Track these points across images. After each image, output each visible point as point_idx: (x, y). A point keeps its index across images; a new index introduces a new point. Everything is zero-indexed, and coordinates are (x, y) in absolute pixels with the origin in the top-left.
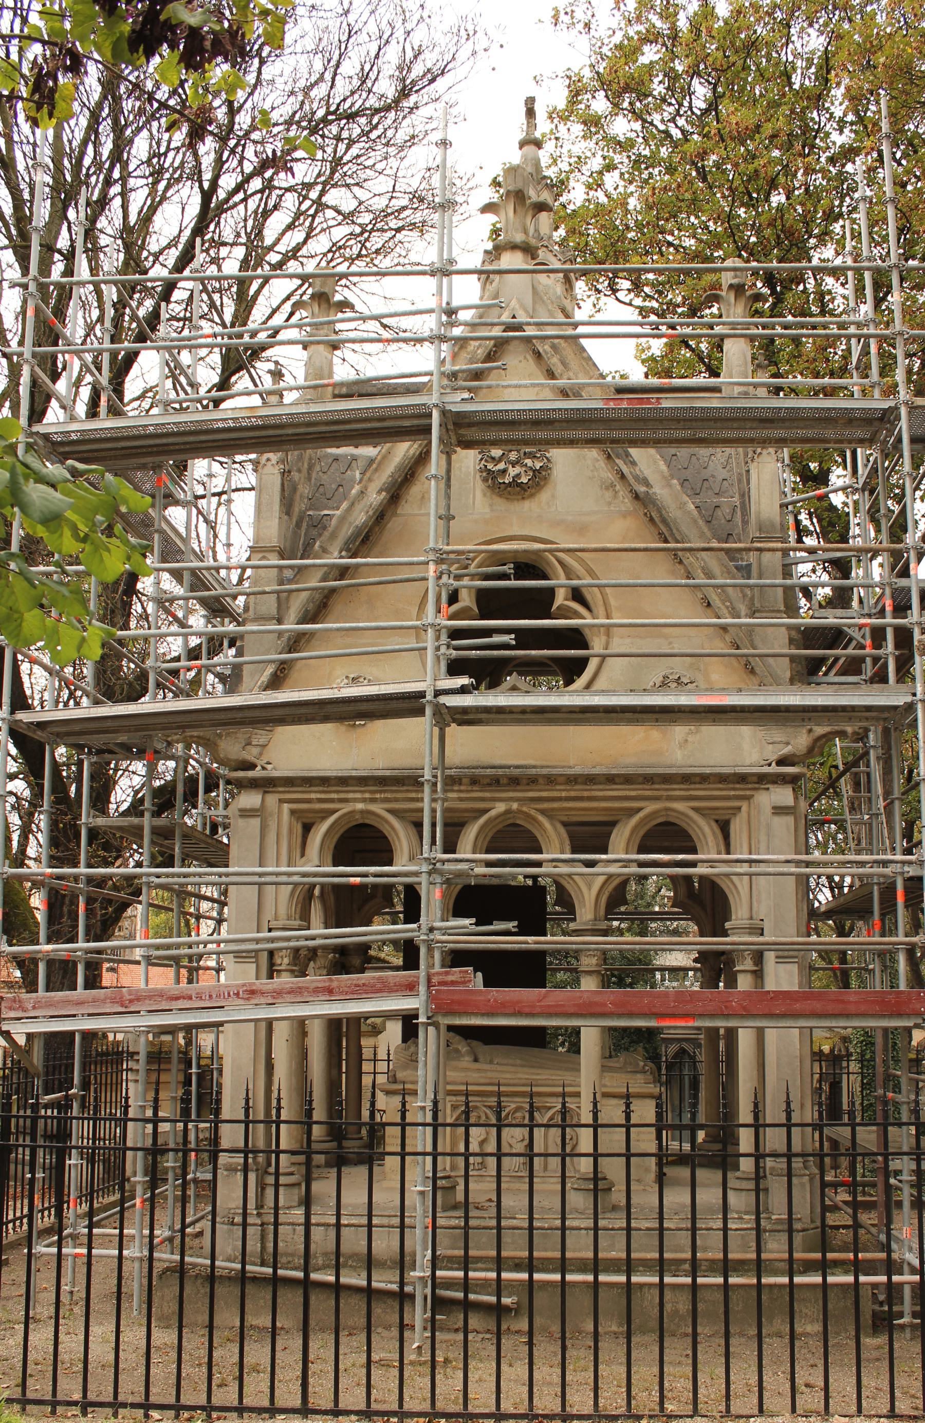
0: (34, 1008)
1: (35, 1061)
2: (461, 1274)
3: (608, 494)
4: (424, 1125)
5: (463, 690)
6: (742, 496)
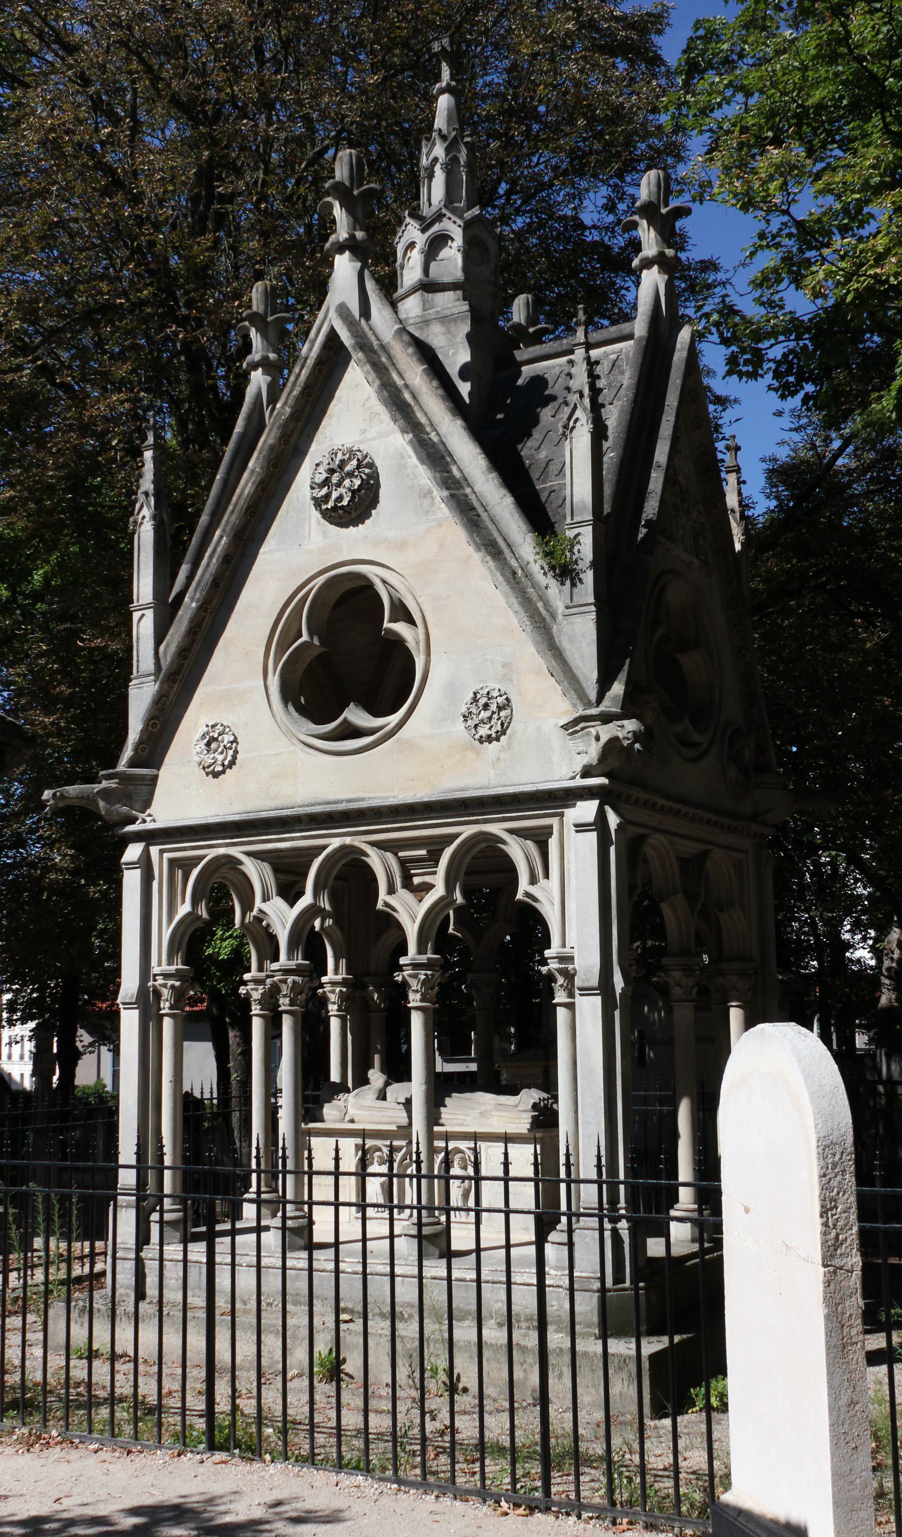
3: (426, 502)
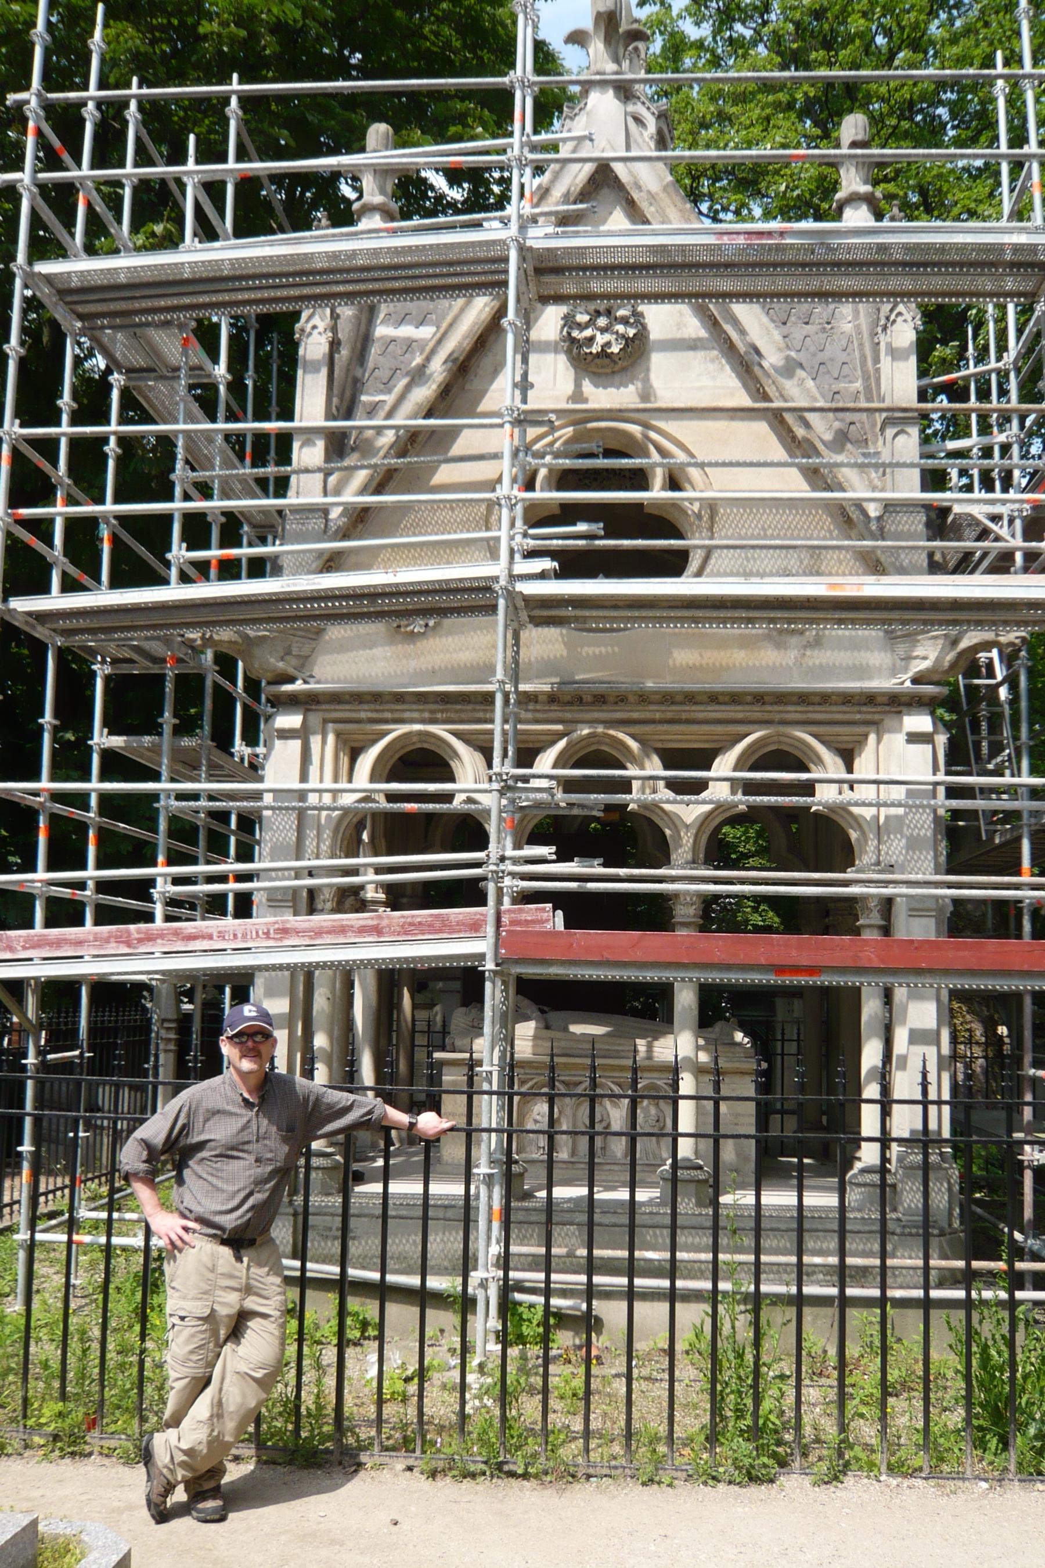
0: (24, 948)
1: (30, 1015)
2: (624, 1281)
4: (490, 1093)
5: (542, 576)
6: (866, 377)
